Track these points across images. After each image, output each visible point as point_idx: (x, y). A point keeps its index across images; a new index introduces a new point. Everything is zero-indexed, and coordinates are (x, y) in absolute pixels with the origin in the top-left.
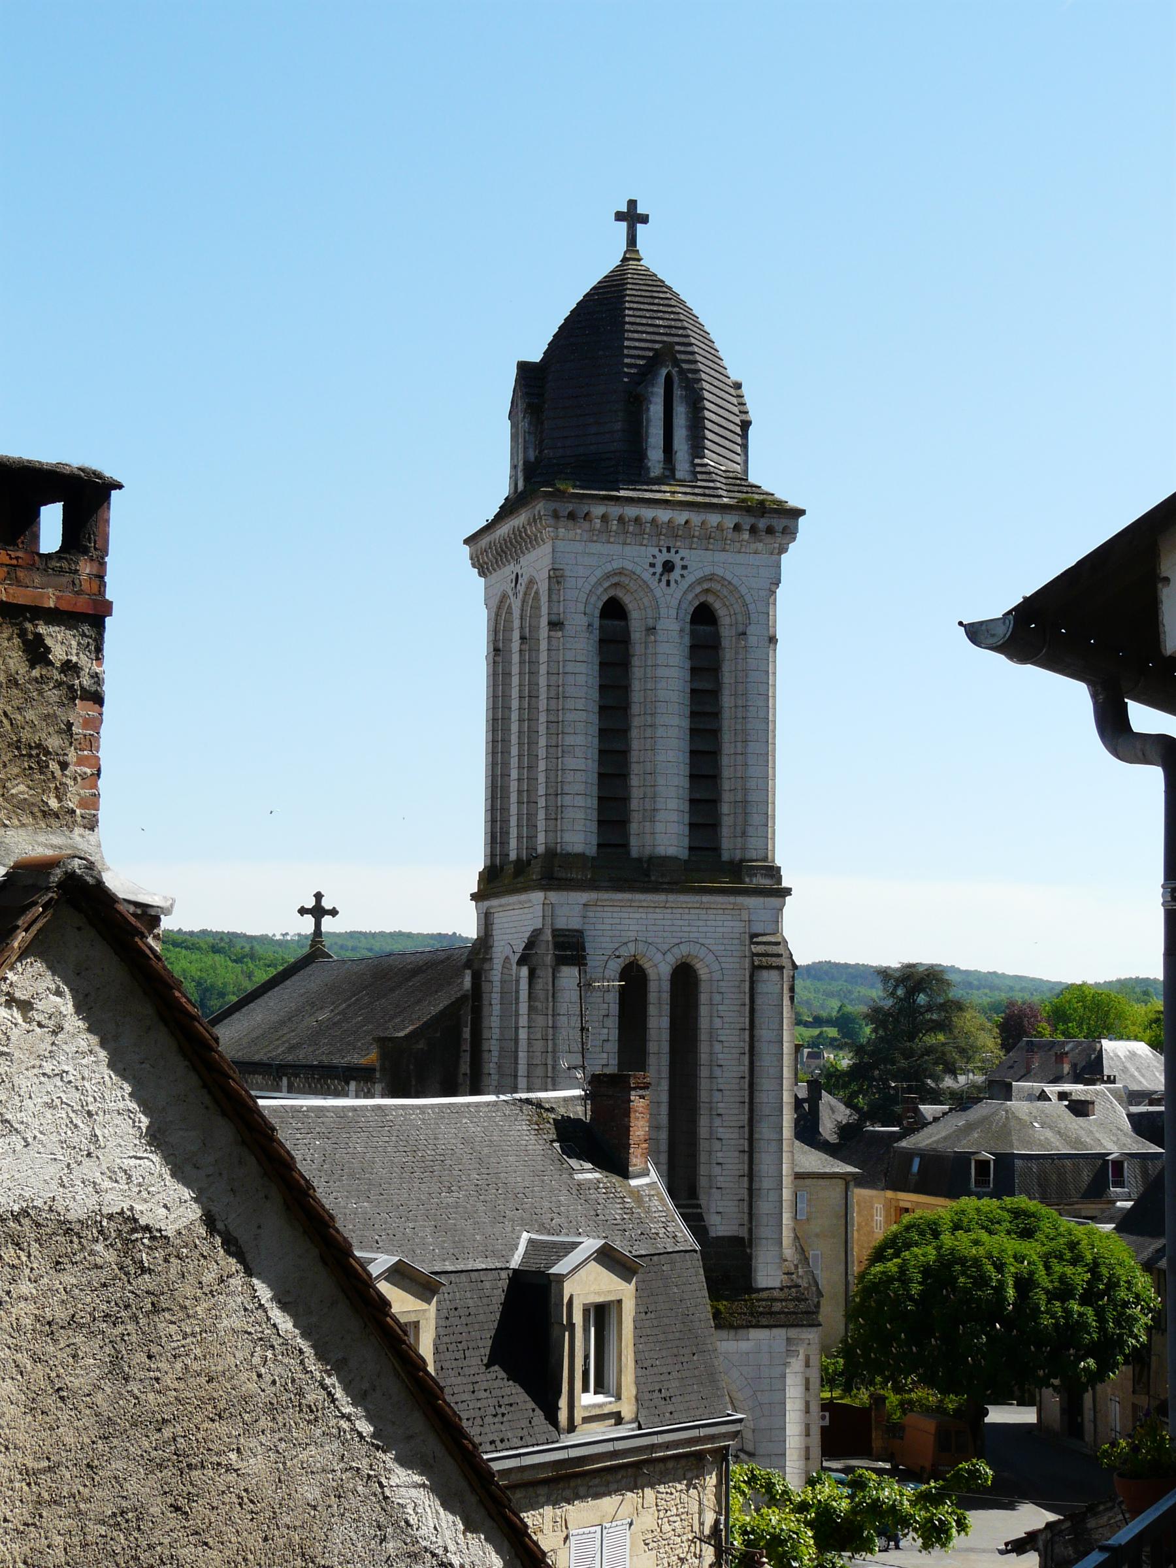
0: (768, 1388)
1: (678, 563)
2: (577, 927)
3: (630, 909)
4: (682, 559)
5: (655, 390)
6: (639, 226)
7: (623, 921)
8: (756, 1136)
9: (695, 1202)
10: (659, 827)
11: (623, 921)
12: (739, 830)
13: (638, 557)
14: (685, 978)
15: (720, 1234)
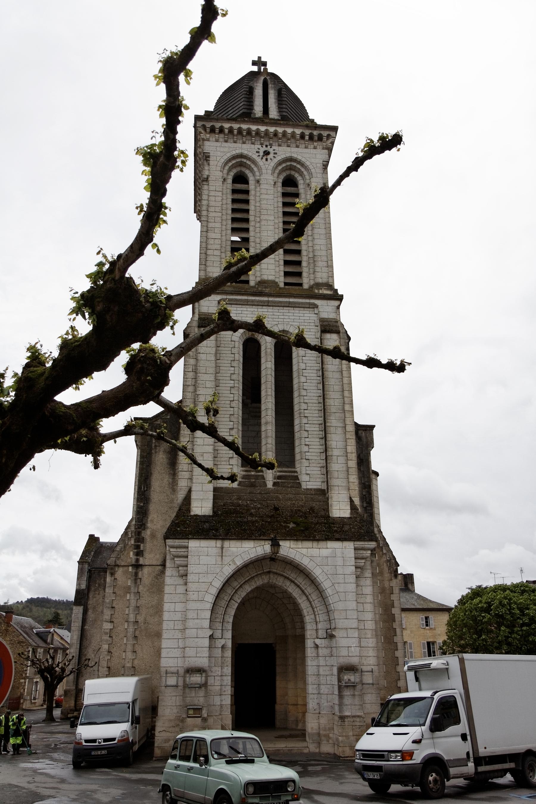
0: (342, 581)
3: (247, 306)
5: (258, 84)
7: (243, 312)
8: (328, 424)
11: (243, 312)
12: (311, 270)
13: (250, 149)
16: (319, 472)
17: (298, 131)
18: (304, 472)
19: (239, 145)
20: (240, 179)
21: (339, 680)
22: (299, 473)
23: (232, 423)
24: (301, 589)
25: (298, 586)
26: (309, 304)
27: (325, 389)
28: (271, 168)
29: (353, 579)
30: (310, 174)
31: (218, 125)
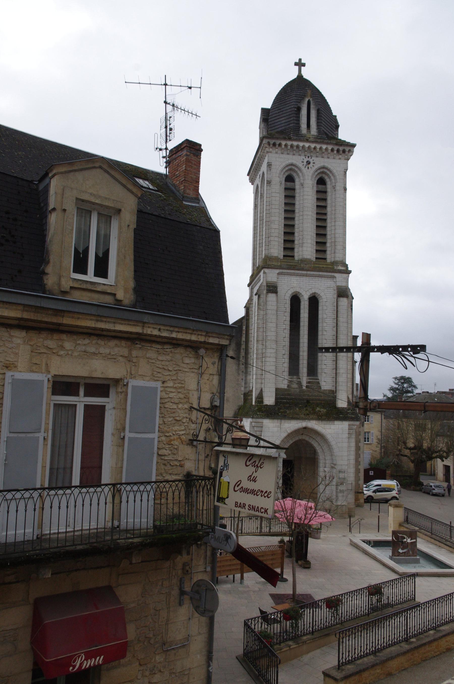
1: (312, 162)
2: (275, 281)
4: (313, 160)
6: (302, 68)
9: (231, 204)
10: (305, 249)
12: (333, 251)
13: (298, 160)
14: (314, 301)
15: (325, 389)
16: (331, 381)
17: (330, 147)
18: (323, 380)
19: (290, 156)
20: (290, 179)
21: (337, 489)
22: (320, 380)
23: (284, 351)
24: (318, 443)
25: (317, 441)
26: (331, 276)
27: (338, 333)
28: (310, 174)
29: (346, 440)
30: (335, 179)
31: (278, 142)
